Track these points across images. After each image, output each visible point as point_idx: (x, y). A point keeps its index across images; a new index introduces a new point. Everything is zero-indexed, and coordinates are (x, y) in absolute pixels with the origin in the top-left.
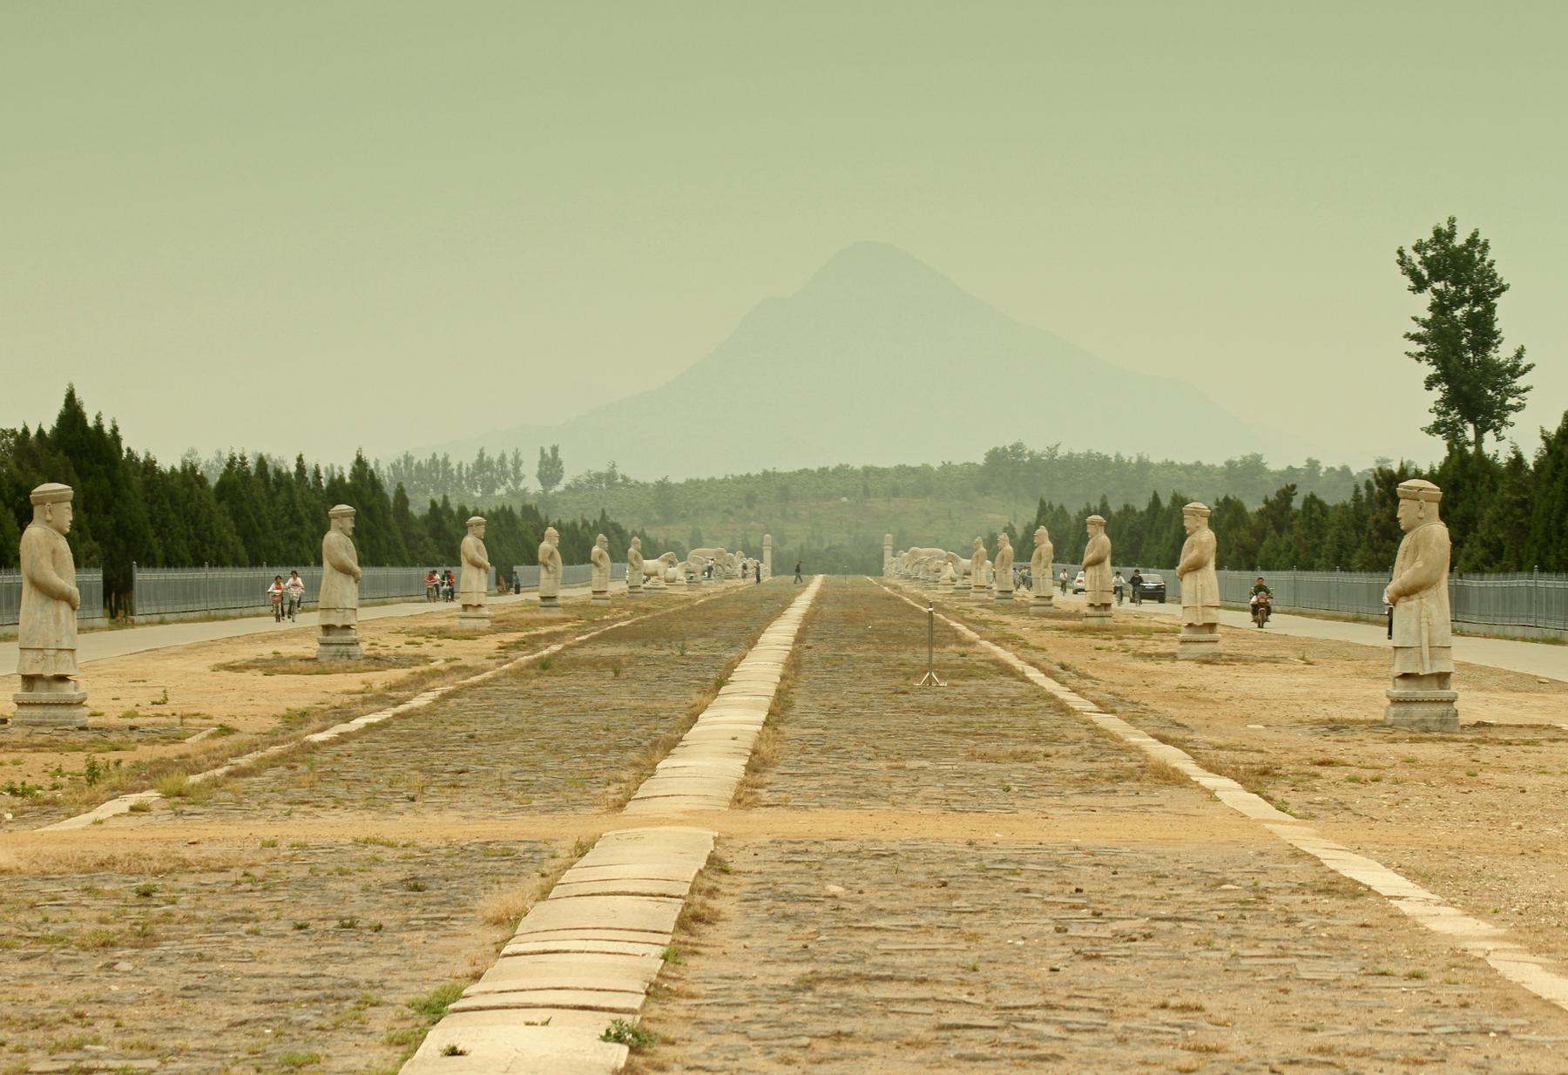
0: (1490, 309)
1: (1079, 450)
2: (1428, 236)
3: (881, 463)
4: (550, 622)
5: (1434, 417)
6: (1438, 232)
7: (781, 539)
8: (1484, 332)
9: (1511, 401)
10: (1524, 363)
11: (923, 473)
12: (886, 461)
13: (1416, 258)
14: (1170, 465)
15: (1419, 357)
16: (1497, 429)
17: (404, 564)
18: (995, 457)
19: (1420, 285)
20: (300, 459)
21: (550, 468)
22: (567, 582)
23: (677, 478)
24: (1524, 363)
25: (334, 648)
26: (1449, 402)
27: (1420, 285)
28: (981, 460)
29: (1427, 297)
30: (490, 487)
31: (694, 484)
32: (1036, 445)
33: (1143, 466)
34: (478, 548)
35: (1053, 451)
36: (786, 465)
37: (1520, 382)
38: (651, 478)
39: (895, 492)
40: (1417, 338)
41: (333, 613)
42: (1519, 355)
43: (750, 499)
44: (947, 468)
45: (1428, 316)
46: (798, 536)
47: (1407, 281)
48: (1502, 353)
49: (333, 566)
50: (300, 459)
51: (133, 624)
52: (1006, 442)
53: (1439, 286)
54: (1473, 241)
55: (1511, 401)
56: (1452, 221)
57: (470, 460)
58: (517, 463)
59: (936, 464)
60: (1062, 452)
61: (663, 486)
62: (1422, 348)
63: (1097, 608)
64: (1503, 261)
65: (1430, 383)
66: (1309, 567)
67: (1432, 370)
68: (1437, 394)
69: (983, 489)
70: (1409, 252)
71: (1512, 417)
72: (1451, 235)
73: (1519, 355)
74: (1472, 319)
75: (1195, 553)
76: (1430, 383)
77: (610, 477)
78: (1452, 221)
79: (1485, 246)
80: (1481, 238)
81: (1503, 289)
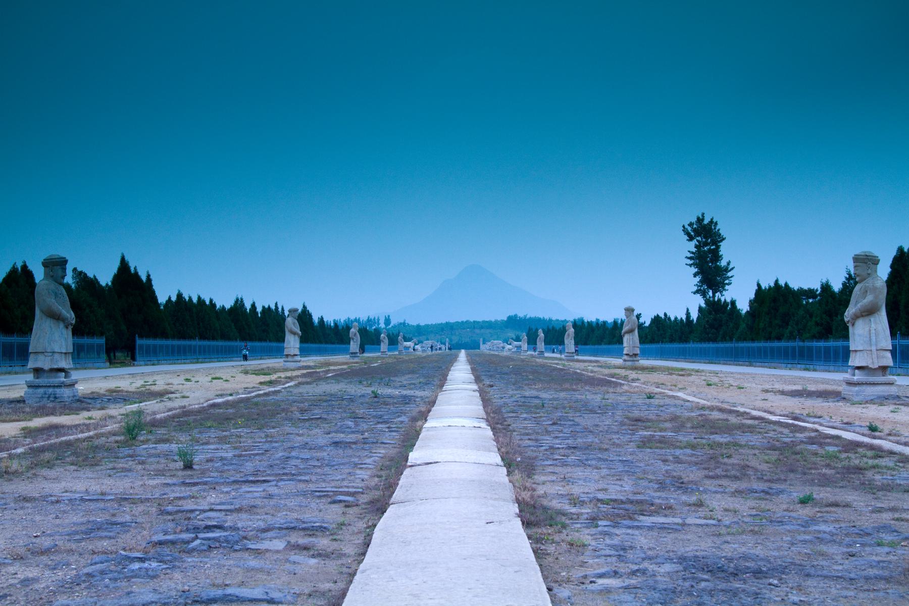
0: (718, 247)
1: (533, 316)
2: (694, 220)
3: (478, 320)
4: (286, 370)
5: (695, 288)
6: (698, 218)
7: (451, 340)
8: (716, 256)
9: (727, 282)
10: (731, 267)
11: (490, 323)
12: (480, 319)
13: (689, 229)
14: (557, 320)
15: (690, 265)
16: (721, 292)
17: (321, 342)
18: (510, 318)
19: (691, 238)
20: (276, 304)
21: (388, 321)
22: (389, 350)
23: (422, 324)
24: (731, 267)
25: (41, 391)
26: (702, 282)
27: (691, 238)
28: (505, 319)
29: (695, 242)
30: (371, 326)
31: (427, 326)
32: (521, 315)
33: (550, 320)
34: (294, 324)
35: (525, 316)
36: (453, 319)
37: (729, 274)
38: (415, 324)
39: (482, 328)
40: (690, 258)
41: (41, 357)
42: (729, 264)
43: (442, 330)
44: (496, 321)
45: (694, 250)
46: (455, 339)
47: (686, 237)
48: (723, 263)
49: (42, 311)
50: (276, 304)
51: (134, 365)
52: (513, 314)
53: (699, 238)
54: (711, 222)
55: (727, 282)
56: (703, 214)
57: (366, 319)
58: (378, 320)
59: (493, 320)
60: (528, 317)
61: (418, 326)
62: (692, 262)
63: (631, 356)
64: (723, 228)
65: (695, 275)
66: (686, 341)
67: (696, 270)
68: (698, 279)
69: (507, 327)
70: (687, 226)
71: (727, 287)
72: (703, 220)
73: (729, 264)
74: (710, 251)
75: (869, 298)
76: (695, 275)
77: (404, 323)
78: (703, 214)
79: (716, 223)
80: (714, 220)
81: (724, 239)
